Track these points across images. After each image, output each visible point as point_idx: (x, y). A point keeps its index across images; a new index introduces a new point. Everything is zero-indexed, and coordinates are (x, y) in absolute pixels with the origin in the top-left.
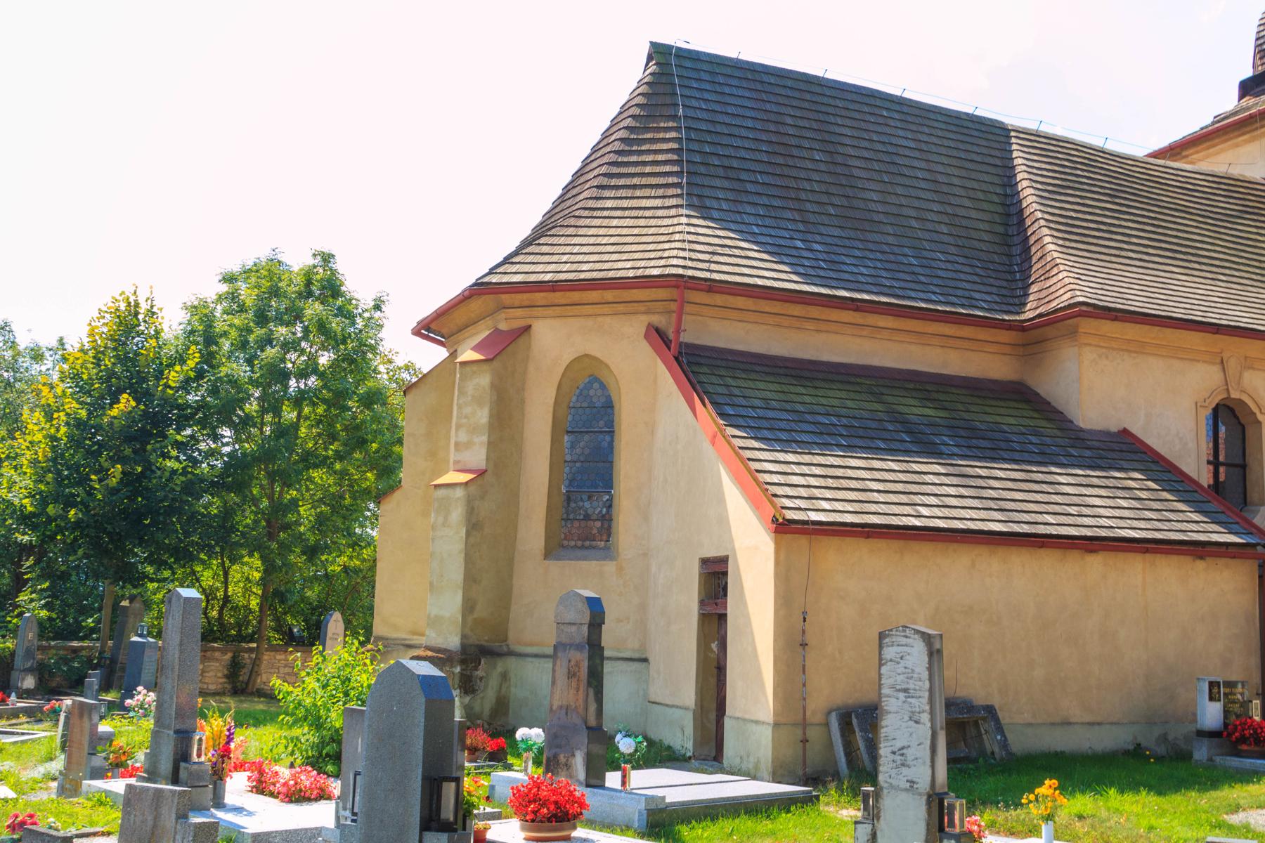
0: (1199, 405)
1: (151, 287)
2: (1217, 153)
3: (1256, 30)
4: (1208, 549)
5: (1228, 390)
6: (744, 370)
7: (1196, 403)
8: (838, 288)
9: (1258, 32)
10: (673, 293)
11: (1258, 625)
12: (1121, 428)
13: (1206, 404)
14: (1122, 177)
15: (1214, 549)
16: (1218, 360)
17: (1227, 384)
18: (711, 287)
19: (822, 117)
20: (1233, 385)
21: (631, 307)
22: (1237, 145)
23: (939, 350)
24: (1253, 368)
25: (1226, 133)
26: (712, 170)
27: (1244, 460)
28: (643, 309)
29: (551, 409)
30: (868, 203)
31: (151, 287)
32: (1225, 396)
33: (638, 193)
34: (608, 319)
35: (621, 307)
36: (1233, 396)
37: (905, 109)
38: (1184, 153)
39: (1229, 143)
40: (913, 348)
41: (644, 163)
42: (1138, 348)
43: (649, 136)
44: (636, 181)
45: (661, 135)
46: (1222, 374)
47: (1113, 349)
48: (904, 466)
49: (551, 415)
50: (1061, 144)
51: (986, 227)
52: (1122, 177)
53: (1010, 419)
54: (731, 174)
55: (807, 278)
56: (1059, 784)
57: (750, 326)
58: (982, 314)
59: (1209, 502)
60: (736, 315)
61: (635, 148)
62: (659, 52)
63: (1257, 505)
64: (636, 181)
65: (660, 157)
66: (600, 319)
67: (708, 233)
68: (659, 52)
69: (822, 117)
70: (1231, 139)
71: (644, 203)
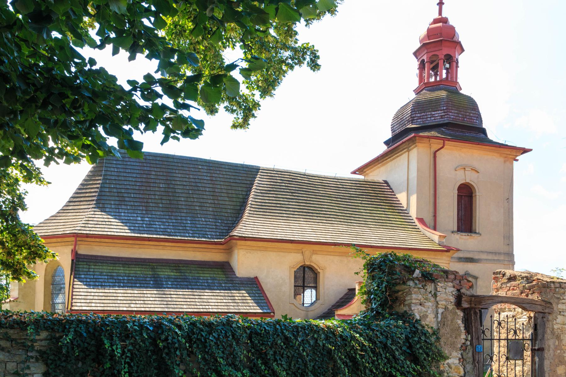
2: (374, 171)
4: (248, 314)
6: (101, 263)
8: (144, 234)
10: (73, 239)
12: (255, 276)
14: (303, 184)
15: (252, 314)
16: (301, 252)
18: (87, 236)
19: (169, 171)
21: (67, 243)
23: (192, 252)
24: (317, 254)
25: (374, 163)
26: (112, 194)
28: (70, 244)
29: (44, 277)
30: (179, 202)
32: (304, 264)
33: (81, 203)
34: (60, 247)
35: (63, 244)
37: (211, 165)
38: (364, 170)
40: (181, 252)
41: (86, 193)
42: (266, 249)
43: (91, 182)
44: (82, 199)
45: (95, 182)
47: (253, 250)
48: (139, 292)
49: (43, 280)
50: (283, 173)
51: (232, 207)
52: (303, 184)
53: (220, 276)
54: (120, 195)
55: (133, 231)
57: (111, 248)
58: (204, 240)
60: (105, 244)
61: (85, 187)
62: (48, 167)
64: (82, 199)
65: (93, 190)
66: (57, 247)
67: (100, 216)
68: (48, 167)
69: (169, 171)
70: (376, 165)
71: (82, 207)
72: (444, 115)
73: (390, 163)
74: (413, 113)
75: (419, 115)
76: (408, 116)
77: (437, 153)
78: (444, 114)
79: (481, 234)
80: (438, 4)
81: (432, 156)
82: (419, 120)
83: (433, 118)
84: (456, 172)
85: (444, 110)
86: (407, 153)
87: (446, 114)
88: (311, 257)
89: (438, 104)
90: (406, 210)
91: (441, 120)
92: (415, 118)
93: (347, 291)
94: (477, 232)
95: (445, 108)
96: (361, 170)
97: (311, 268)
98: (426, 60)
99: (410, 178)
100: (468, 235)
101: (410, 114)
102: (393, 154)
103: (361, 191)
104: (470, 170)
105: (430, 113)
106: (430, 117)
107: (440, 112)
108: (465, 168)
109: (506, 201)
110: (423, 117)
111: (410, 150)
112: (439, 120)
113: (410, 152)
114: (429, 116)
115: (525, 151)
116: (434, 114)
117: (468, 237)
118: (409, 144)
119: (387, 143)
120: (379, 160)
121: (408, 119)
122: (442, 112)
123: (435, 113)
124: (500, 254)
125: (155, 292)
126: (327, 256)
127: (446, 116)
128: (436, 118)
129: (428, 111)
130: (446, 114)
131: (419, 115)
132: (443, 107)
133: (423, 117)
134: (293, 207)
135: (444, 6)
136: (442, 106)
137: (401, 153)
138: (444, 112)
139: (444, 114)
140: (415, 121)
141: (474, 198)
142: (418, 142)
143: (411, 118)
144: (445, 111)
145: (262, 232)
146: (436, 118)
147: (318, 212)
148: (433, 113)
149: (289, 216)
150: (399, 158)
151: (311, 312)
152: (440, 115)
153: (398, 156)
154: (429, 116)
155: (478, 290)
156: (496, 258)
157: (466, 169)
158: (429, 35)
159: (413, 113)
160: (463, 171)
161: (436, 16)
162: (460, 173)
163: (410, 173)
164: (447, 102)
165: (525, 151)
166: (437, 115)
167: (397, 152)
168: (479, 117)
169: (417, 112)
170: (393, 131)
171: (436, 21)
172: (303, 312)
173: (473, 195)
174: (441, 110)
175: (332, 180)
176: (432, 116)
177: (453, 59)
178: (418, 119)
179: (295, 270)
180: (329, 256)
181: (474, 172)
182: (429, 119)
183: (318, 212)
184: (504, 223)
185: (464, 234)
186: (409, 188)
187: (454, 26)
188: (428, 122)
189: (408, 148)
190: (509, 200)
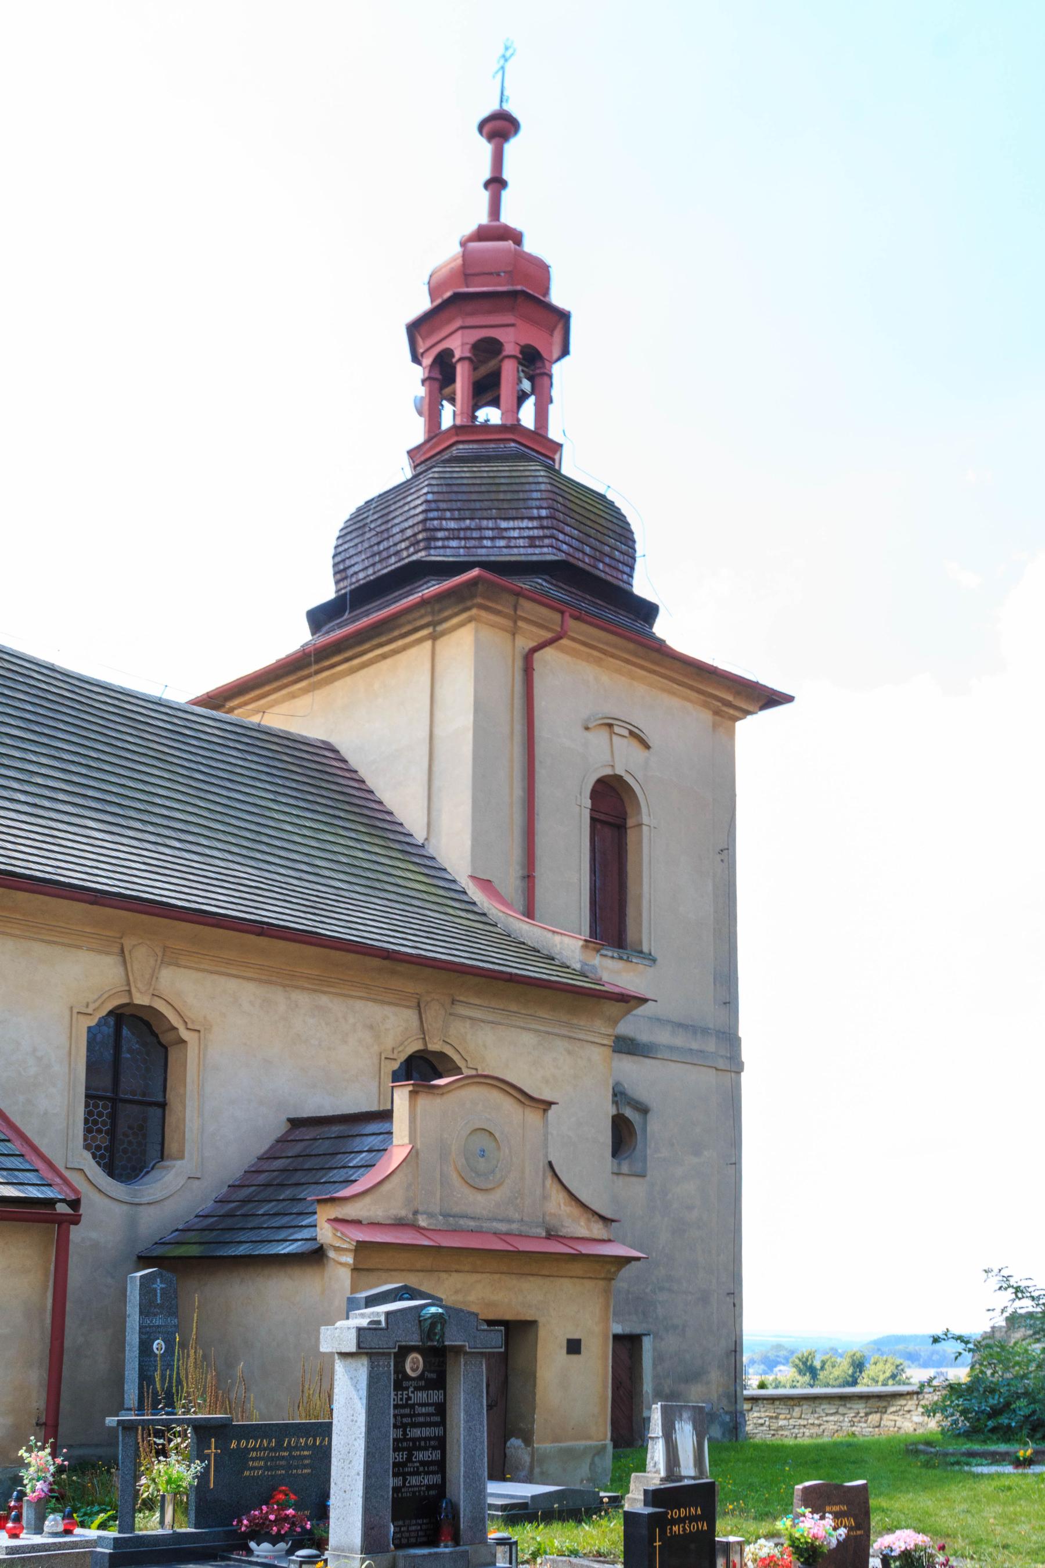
0: (75, 1010)
1: (989, 1310)
3: (334, 543)
5: (129, 991)
7: (71, 1008)
9: (336, 547)
11: (48, 1321)
13: (90, 1011)
17: (129, 984)
20: (139, 985)
22: (293, 696)
27: (165, 1097)
31: (989, 1310)
32: (125, 1000)
36: (137, 1001)
39: (284, 692)
46: (121, 970)
56: (595, 1514)
59: (9, 1141)
63: (175, 1159)
70: (286, 686)
72: (539, 538)
73: (348, 680)
74: (431, 515)
75: (452, 524)
76: (410, 522)
77: (537, 655)
78: (540, 533)
79: (654, 960)
80: (487, 185)
81: (519, 664)
82: (454, 543)
83: (502, 543)
84: (587, 734)
85: (540, 518)
86: (428, 644)
87: (547, 532)
88: (154, 976)
89: (521, 496)
90: (423, 846)
91: (530, 551)
92: (440, 534)
93: (283, 1128)
94: (645, 949)
95: (544, 513)
96: (218, 699)
97: (148, 1025)
98: (458, 354)
99: (437, 731)
100: (621, 958)
101: (421, 517)
102: (367, 646)
103: (262, 761)
104: (626, 733)
105: (491, 524)
106: (492, 539)
107: (525, 523)
108: (610, 726)
109: (719, 857)
110: (468, 534)
111: (443, 634)
112: (522, 551)
113: (441, 643)
114: (489, 533)
115: (771, 699)
116: (506, 529)
117: (620, 965)
118: (441, 611)
119: (319, 618)
120: (309, 665)
121: (409, 532)
122: (535, 523)
123: (511, 524)
124: (705, 1031)
125: (92, 931)
126: (216, 977)
127: (547, 541)
128: (513, 543)
129: (485, 514)
130: (547, 532)
131: (452, 524)
132: (539, 508)
133: (468, 534)
134: (43, 771)
135: (505, 195)
136: (534, 503)
137: (400, 643)
138: (542, 527)
139: (540, 533)
140: (440, 544)
141: (631, 836)
142: (481, 607)
143: (425, 530)
144: (545, 523)
145: (235, 753)
146: (513, 543)
147: (138, 805)
148: (504, 524)
149: (37, 801)
150: (389, 661)
151: (151, 1210)
152: (526, 533)
153: (384, 657)
154: (489, 533)
155: (649, 1152)
156: (695, 1046)
157: (617, 729)
158: (469, 272)
159: (431, 515)
160: (604, 733)
161: (484, 219)
162: (599, 739)
163: (439, 716)
164: (551, 495)
165: (771, 699)
166: (516, 534)
167: (384, 639)
168: (630, 563)
169: (448, 514)
170: (340, 572)
171: (482, 234)
172: (118, 1209)
173: (630, 822)
174: (531, 518)
175: (150, 706)
176: (500, 534)
177: (544, 367)
178: (448, 539)
179: (93, 1022)
180: (222, 980)
181: (634, 743)
182: (486, 543)
183: (138, 805)
184: (714, 929)
185: (610, 954)
186: (435, 769)
187: (548, 260)
188: (483, 551)
189: (434, 624)
190: (726, 853)
